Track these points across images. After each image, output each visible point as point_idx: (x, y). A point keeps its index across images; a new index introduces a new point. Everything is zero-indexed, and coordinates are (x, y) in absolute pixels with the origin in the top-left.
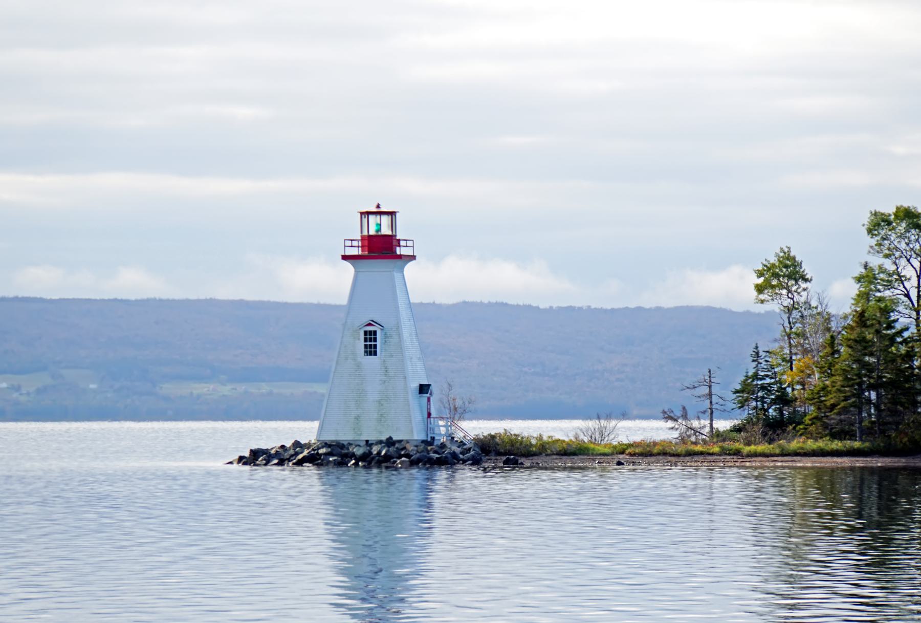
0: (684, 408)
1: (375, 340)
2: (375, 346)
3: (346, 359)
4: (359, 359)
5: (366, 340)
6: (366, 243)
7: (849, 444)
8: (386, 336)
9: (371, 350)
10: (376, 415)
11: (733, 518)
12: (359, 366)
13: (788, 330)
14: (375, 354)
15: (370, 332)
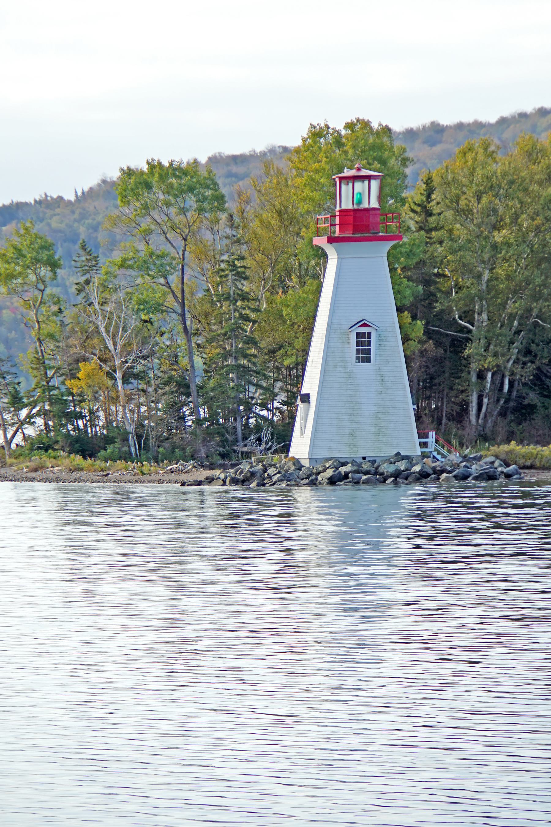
1: (369, 344)
2: (369, 351)
3: (336, 367)
5: (358, 344)
8: (380, 338)
9: (364, 356)
13: (533, 539)
14: (369, 360)
15: (364, 334)
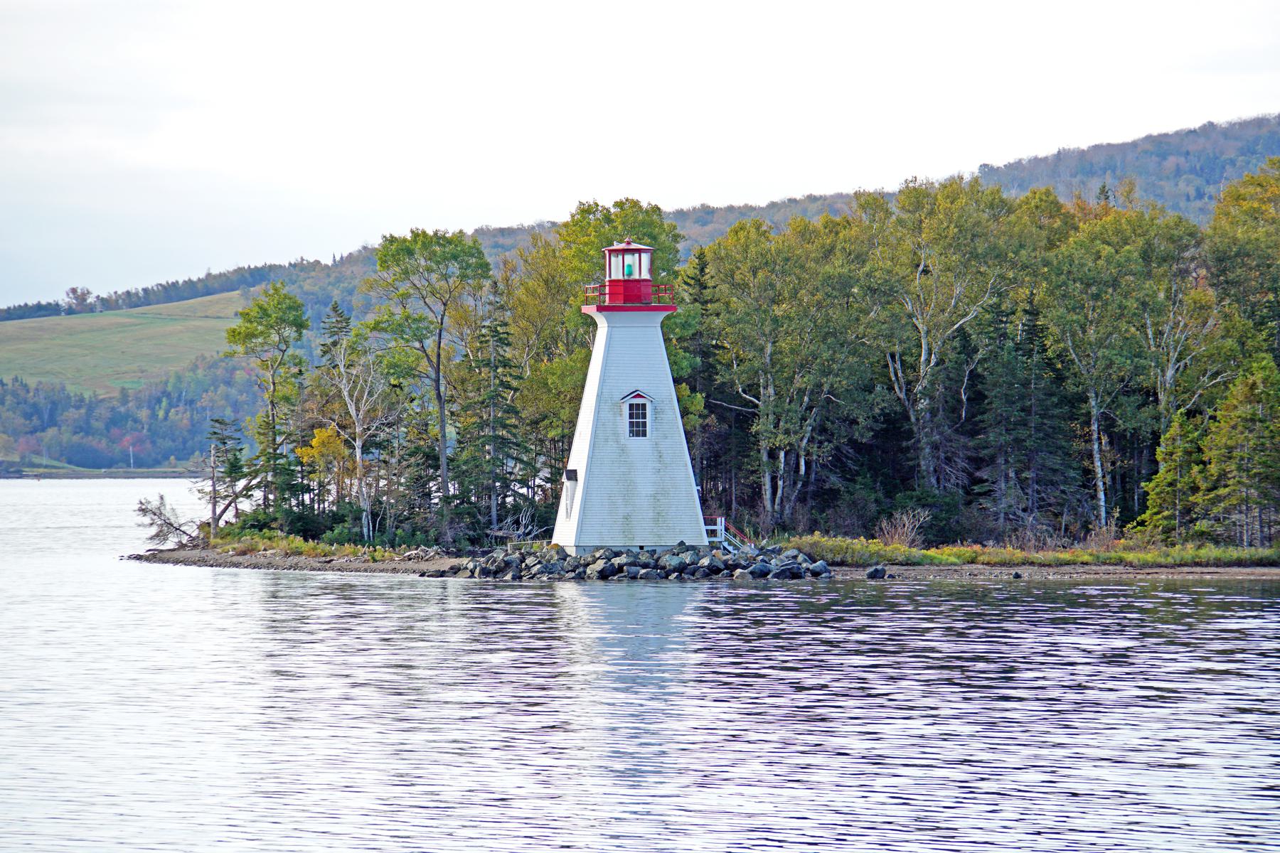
0: (162, 498)
1: (644, 416)
3: (606, 440)
4: (623, 441)
5: (631, 416)
6: (621, 290)
7: (1233, 553)
9: (638, 429)
10: (651, 515)
11: (417, 822)
12: (623, 450)
14: (644, 435)
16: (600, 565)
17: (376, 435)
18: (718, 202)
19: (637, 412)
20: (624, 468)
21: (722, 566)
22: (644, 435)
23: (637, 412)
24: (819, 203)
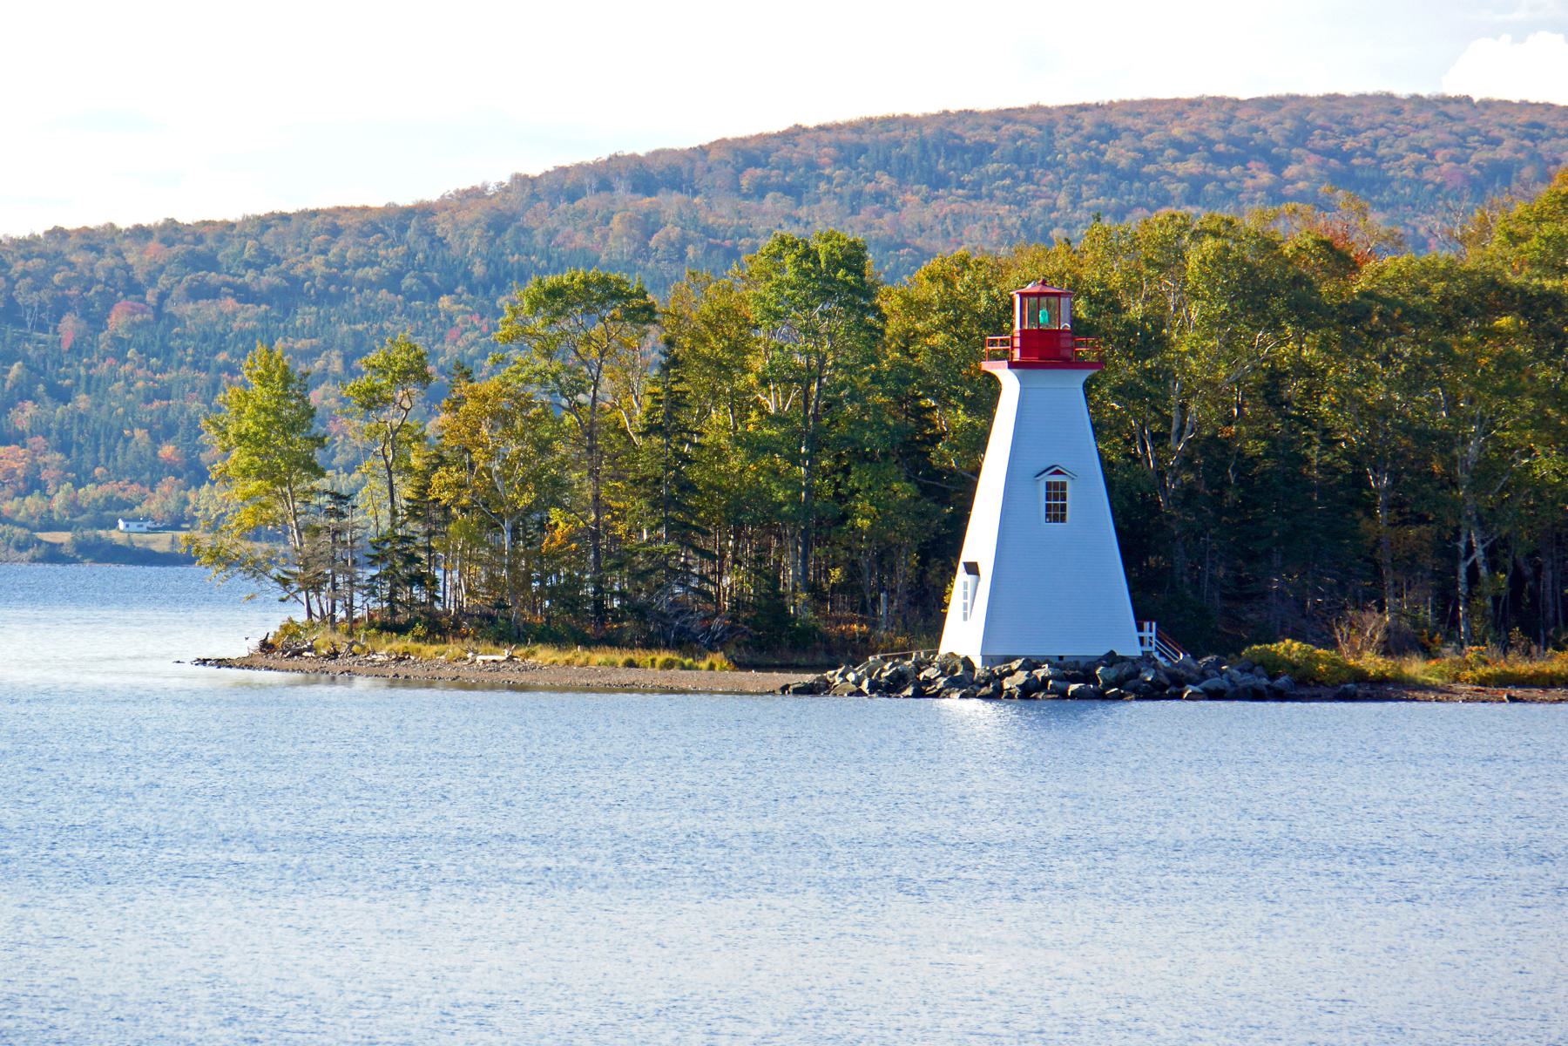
5: (1064, 507)
9: (1056, 513)
14: (1063, 520)
16: (1021, 677)
17: (704, 473)
18: (187, 217)
19: (1056, 493)
20: (1017, 544)
21: (1167, 682)
22: (1063, 520)
23: (1056, 493)
24: (318, 219)
